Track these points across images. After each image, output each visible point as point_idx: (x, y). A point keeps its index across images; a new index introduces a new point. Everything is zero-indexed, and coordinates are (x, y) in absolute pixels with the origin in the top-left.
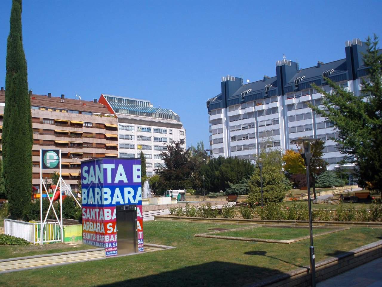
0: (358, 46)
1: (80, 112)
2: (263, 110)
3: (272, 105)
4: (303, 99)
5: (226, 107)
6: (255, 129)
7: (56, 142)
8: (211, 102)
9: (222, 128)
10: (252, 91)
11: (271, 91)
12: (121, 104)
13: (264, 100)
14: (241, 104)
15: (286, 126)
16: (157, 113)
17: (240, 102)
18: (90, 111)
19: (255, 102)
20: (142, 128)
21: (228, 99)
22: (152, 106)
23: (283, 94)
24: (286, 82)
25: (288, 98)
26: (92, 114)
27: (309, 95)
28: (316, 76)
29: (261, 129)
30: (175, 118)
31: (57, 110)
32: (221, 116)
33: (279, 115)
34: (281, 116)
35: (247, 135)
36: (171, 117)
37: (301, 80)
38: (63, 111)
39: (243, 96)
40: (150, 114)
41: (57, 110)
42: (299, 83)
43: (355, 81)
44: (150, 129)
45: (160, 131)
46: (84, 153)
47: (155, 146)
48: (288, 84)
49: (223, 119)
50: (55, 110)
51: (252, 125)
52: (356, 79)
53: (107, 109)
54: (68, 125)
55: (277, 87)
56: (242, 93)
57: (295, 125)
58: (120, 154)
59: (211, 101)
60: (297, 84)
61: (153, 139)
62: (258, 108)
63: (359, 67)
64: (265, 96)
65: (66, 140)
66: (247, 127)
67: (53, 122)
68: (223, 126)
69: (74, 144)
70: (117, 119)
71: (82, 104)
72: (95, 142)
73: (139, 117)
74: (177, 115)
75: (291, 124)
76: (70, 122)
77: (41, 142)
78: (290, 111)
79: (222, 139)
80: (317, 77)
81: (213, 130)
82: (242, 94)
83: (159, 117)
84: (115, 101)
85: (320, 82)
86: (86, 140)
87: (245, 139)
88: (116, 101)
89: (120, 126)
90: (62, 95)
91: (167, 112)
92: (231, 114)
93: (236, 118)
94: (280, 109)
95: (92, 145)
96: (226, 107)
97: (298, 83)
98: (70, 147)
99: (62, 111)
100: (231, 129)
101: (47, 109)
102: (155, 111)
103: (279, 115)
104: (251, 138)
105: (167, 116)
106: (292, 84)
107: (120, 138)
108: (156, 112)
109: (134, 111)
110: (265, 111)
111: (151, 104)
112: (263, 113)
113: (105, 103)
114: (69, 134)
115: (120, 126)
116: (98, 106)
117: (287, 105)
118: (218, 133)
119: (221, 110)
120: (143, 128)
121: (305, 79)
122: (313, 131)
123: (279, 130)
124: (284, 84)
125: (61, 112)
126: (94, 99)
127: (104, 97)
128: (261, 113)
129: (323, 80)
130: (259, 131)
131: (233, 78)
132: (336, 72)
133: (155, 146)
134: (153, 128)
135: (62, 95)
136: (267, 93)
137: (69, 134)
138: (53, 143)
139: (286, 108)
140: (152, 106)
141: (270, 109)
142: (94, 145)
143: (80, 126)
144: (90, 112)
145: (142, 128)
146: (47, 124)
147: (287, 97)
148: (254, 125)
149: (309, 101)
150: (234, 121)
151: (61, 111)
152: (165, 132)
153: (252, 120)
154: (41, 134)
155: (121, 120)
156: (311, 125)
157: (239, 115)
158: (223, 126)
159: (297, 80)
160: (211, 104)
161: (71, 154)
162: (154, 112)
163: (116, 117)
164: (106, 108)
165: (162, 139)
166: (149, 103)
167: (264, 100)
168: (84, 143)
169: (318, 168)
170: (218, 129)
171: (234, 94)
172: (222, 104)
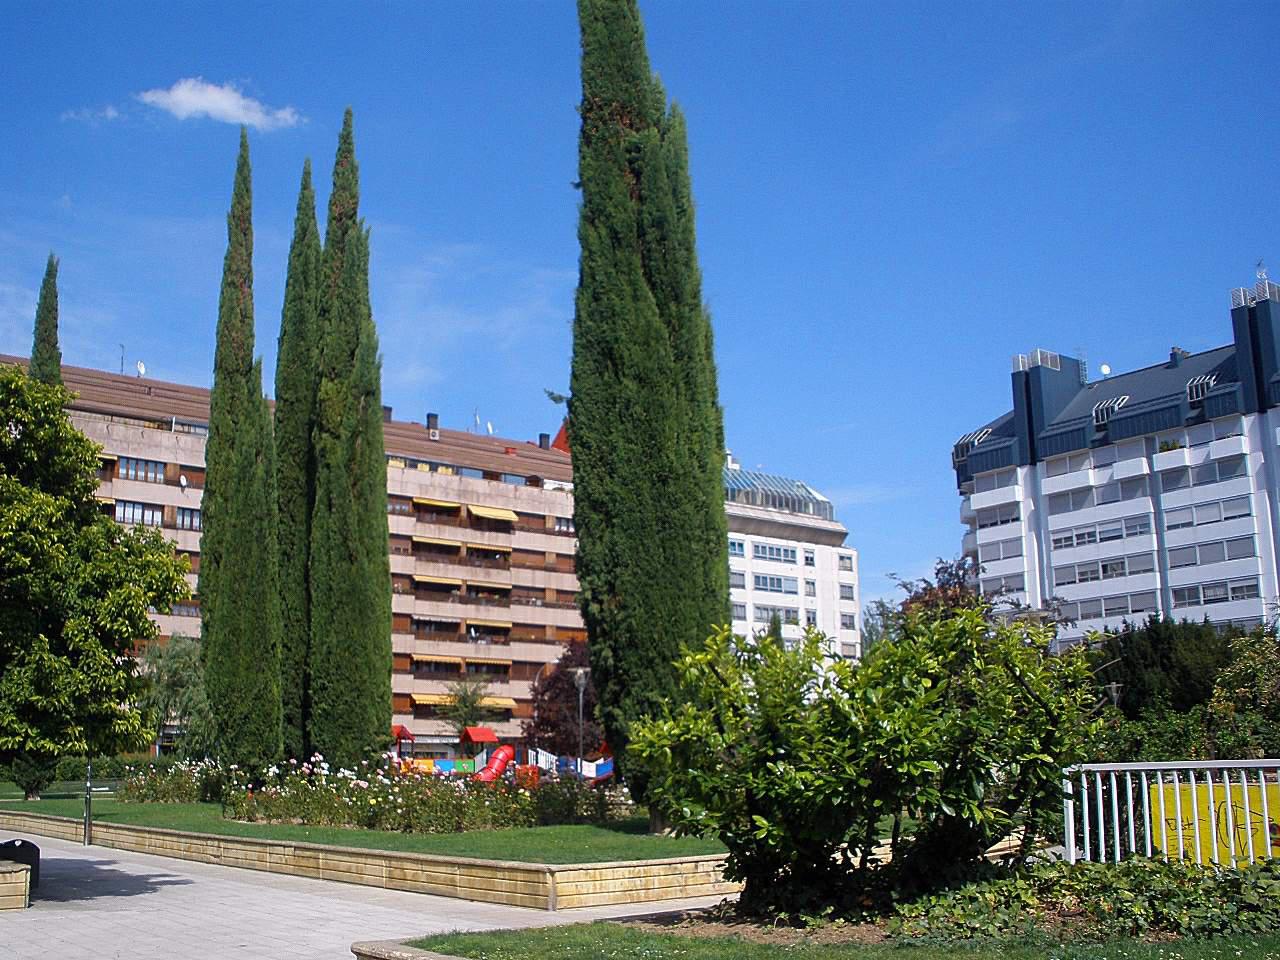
0: (1271, 305)
2: (1182, 471)
3: (1219, 449)
6: (1151, 539)
7: (417, 578)
8: (973, 445)
9: (1020, 539)
10: (1131, 403)
13: (1186, 432)
14: (1094, 448)
17: (1183, 422)
19: (1150, 441)
22: (736, 467)
23: (1033, 461)
29: (1173, 539)
30: (819, 510)
31: (419, 465)
32: (1183, 459)
34: (1259, 488)
36: (806, 506)
37: (1116, 408)
38: (440, 469)
41: (419, 465)
43: (1265, 415)
45: (774, 554)
46: (514, 624)
47: (758, 608)
49: (1021, 505)
50: (413, 464)
51: (1065, 538)
54: (461, 521)
55: (1016, 439)
62: (1164, 461)
63: (1043, 429)
66: (1121, 529)
67: (407, 508)
68: (1022, 528)
69: (478, 589)
74: (827, 500)
75: (1063, 557)
76: (469, 511)
78: (1131, 498)
79: (1021, 575)
81: (982, 546)
83: (767, 503)
85: (1178, 414)
87: (1086, 580)
92: (1054, 484)
93: (1079, 497)
94: (1024, 512)
96: (1033, 463)
97: (1103, 420)
98: (463, 601)
99: (436, 470)
100: (1225, 510)
106: (1179, 399)
108: (754, 485)
110: (1190, 470)
111: (734, 461)
112: (1089, 497)
114: (464, 552)
118: (1004, 558)
119: (1015, 471)
122: (1158, 574)
124: (1266, 371)
125: (435, 474)
126: (429, 416)
128: (1174, 478)
131: (1053, 358)
132: (991, 440)
133: (758, 608)
136: (1099, 428)
137: (464, 552)
138: (407, 585)
139: (1044, 505)
140: (736, 467)
142: (550, 597)
148: (1148, 525)
149: (1141, 478)
150: (995, 524)
151: (434, 467)
152: (790, 557)
153: (1142, 505)
156: (1019, 579)
157: (1089, 488)
158: (1022, 528)
160: (971, 452)
161: (469, 627)
165: (779, 580)
167: (1186, 432)
168: (515, 587)
170: (1003, 542)
171: (1059, 414)
172: (1016, 450)
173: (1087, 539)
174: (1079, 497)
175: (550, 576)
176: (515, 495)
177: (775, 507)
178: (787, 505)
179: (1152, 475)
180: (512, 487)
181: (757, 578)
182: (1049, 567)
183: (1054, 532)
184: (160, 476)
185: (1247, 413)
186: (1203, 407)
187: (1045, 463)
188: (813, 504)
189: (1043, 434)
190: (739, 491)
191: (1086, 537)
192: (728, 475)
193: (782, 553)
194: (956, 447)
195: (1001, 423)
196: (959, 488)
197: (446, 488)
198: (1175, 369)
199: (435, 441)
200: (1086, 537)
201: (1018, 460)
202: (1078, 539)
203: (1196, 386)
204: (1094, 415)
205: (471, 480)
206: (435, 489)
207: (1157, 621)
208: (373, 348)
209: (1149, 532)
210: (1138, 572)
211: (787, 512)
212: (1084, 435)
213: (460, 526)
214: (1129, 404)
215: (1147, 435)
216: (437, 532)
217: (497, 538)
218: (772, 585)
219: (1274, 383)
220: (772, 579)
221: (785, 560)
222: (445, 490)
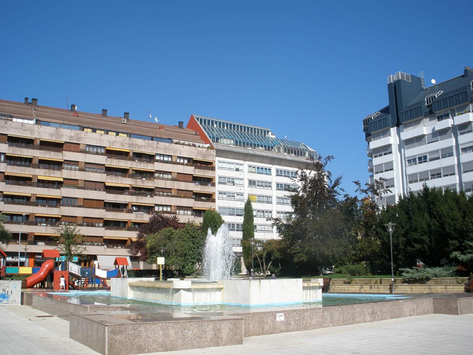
1: (152, 139)
2: (423, 136)
7: (107, 184)
12: (223, 131)
16: (281, 145)
18: (169, 137)
20: (256, 168)
26: (172, 142)
35: (439, 169)
39: (428, 103)
40: (269, 148)
44: (270, 170)
45: (260, 171)
49: (392, 145)
53: (199, 137)
56: (427, 99)
58: (219, 208)
59: (371, 118)
61: (274, 186)
65: (126, 182)
69: (140, 189)
70: (215, 151)
72: (176, 187)
73: (249, 150)
74: (314, 151)
76: (131, 240)
77: (81, 184)
81: (375, 166)
83: (285, 151)
84: (213, 125)
85: (466, 96)
86: (160, 184)
88: (215, 126)
89: (220, 162)
90: (125, 113)
91: (297, 146)
92: (409, 133)
95: (171, 193)
101: (94, 130)
107: (219, 183)
109: (244, 143)
111: (272, 134)
113: (198, 129)
114: (131, 172)
115: (220, 162)
116: (183, 131)
120: (258, 168)
123: (455, 185)
126: (179, 122)
130: (461, 161)
134: (274, 168)
135: (125, 113)
137: (131, 154)
141: (414, 139)
143: (151, 158)
145: (256, 168)
146: (67, 169)
151: (117, 134)
152: (268, 171)
153: (451, 142)
154: (80, 170)
155: (221, 153)
161: (133, 206)
162: (277, 145)
163: (212, 148)
164: (197, 135)
166: (268, 132)
168: (156, 187)
174: (419, 139)
175: (75, 176)
176: (157, 146)
180: (155, 142)
181: (278, 184)
183: (407, 158)
186: (431, 107)
187: (403, 125)
189: (402, 111)
191: (423, 159)
193: (290, 173)
197: (122, 143)
199: (125, 124)
200: (423, 159)
201: (390, 124)
205: (135, 139)
206: (117, 143)
207: (402, 199)
208: (373, 150)
209: (452, 155)
210: (447, 175)
211: (251, 149)
212: (421, 109)
213: (129, 160)
216: (117, 162)
217: (208, 173)
221: (284, 176)
222: (122, 144)
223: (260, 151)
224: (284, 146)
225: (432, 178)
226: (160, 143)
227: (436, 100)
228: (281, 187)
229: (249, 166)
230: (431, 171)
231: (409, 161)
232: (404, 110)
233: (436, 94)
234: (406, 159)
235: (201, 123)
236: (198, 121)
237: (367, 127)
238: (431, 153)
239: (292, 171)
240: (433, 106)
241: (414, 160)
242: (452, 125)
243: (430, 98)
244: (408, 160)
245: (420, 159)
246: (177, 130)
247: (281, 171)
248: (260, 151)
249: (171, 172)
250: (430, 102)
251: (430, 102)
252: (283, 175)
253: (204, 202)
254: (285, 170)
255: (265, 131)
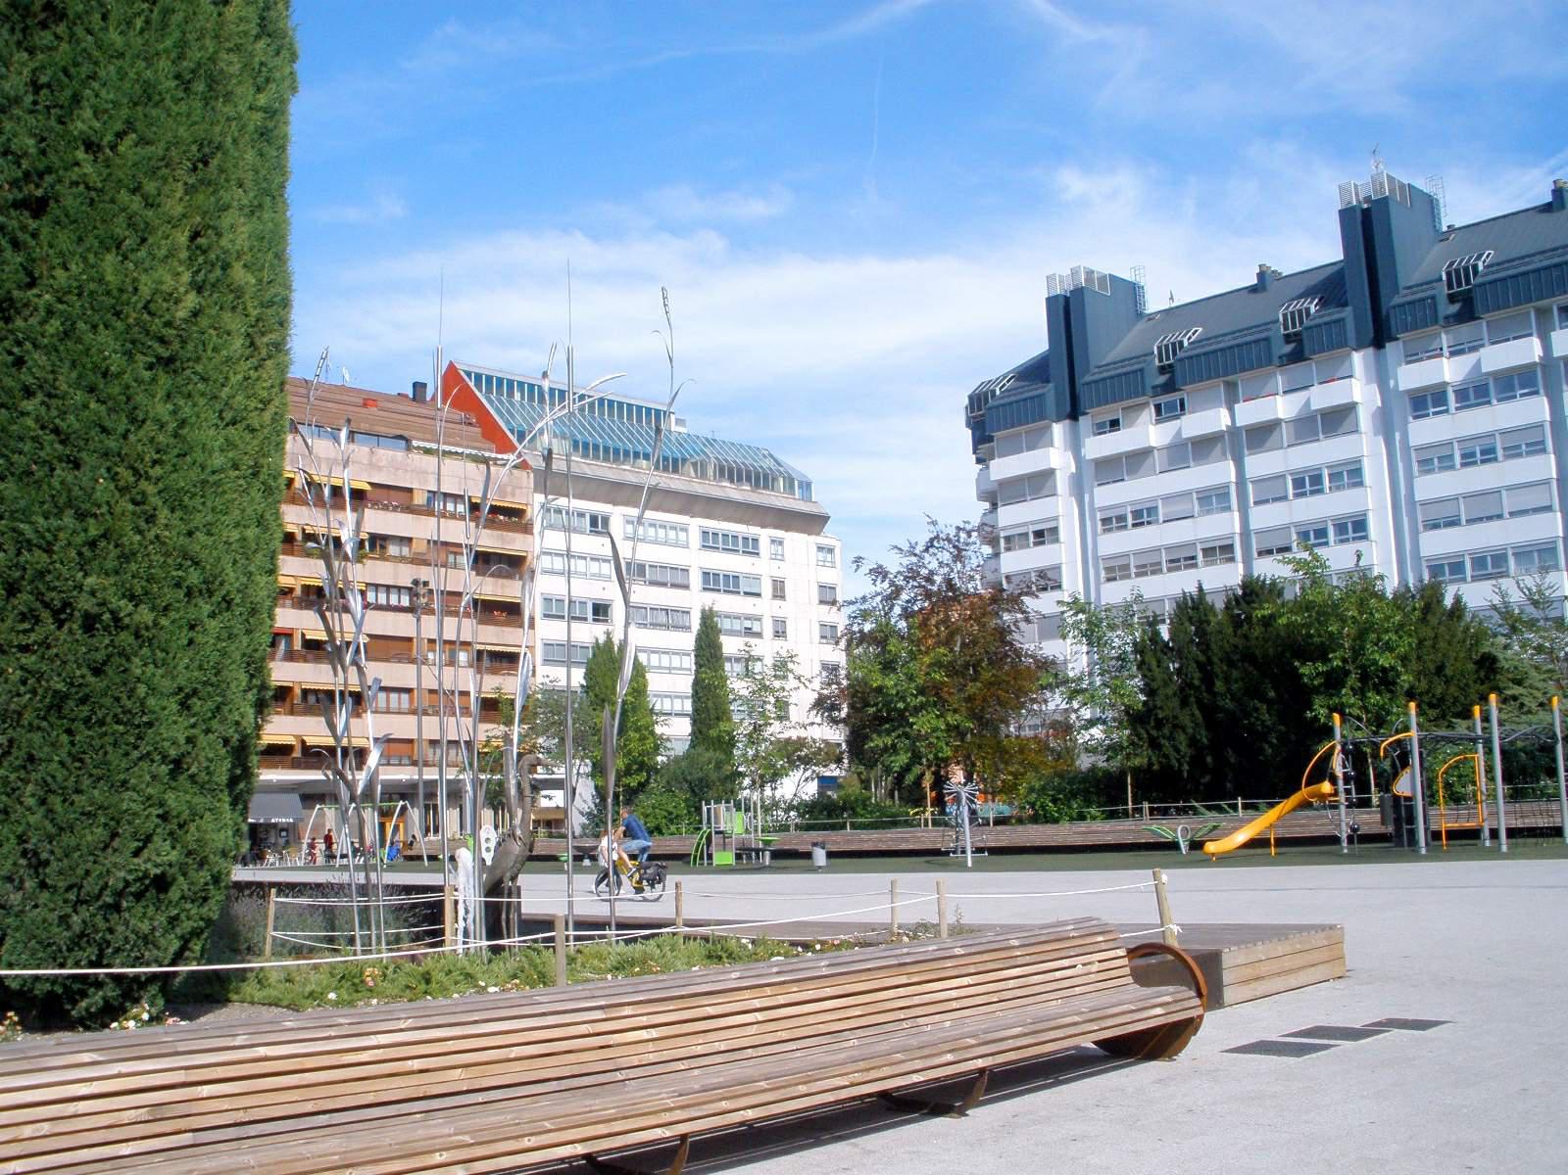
2: (1145, 453)
3: (1323, 396)
4: (1499, 356)
5: (1074, 415)
6: (1233, 519)
11: (997, 407)
15: (1403, 492)
16: (708, 457)
18: (399, 432)
19: (1231, 387)
21: (1084, 376)
23: (1379, 337)
24: (1396, 284)
25: (1412, 357)
27: (1531, 335)
28: (1246, 326)
32: (1275, 410)
33: (1365, 445)
39: (1161, 360)
40: (672, 465)
42: (1301, 322)
48: (1405, 292)
52: (1388, 345)
53: (478, 430)
56: (1159, 348)
57: (1156, 543)
60: (1291, 330)
61: (695, 579)
62: (1249, 413)
64: (1285, 355)
70: (532, 475)
71: (361, 401)
75: (1432, 486)
79: (1057, 568)
80: (1425, 287)
82: (1160, 353)
83: (722, 474)
84: (511, 394)
85: (1269, 348)
88: (517, 396)
93: (1135, 461)
102: (702, 451)
103: (1365, 445)
104: (1436, 526)
105: (749, 473)
110: (1283, 424)
117: (1093, 460)
121: (1200, 341)
124: (1384, 290)
126: (415, 385)
127: (462, 374)
128: (1261, 435)
129: (1282, 340)
130: (1253, 526)
134: (696, 524)
139: (1089, 473)
141: (1121, 458)
144: (401, 437)
147: (1406, 356)
152: (751, 547)
153: (1220, 471)
159: (1457, 271)
162: (698, 454)
164: (470, 424)
169: (1246, 722)
173: (1115, 524)
174: (1135, 461)
176: (370, 461)
177: (732, 481)
178: (749, 479)
179: (1234, 431)
181: (706, 574)
182: (1096, 558)
183: (1101, 509)
184: (405, 705)
185: (1058, 420)
186: (1173, 372)
187: (1400, 343)
188: (784, 478)
189: (1088, 378)
190: (684, 460)
191: (1143, 516)
192: (670, 440)
194: (971, 398)
195: (1026, 368)
196: (974, 453)
198: (1264, 294)
200: (1143, 516)
201: (1352, 342)
202: (1103, 525)
203: (1292, 313)
204: (1156, 352)
212: (1142, 377)
214: (1495, 261)
215: (1539, 303)
218: (727, 584)
219: (1394, 307)
220: (726, 576)
221: (724, 549)
223: (643, 474)
224: (717, 458)
225: (1170, 570)
226: (381, 452)
227: (1187, 354)
228: (717, 582)
229: (819, 548)
230: (1168, 549)
231: (1105, 521)
232: (1094, 374)
233: (1185, 335)
234: (1099, 516)
235: (478, 384)
236: (470, 379)
237: (982, 416)
238: (1167, 499)
239: (746, 535)
240: (1178, 367)
241: (1121, 518)
242: (1227, 426)
243: (1167, 346)
244: (1203, 550)
245: (1137, 514)
246: (409, 409)
247: (745, 539)
248: (643, 474)
249: (410, 539)
250: (1168, 358)
251: (1168, 358)
252: (721, 546)
253: (504, 629)
254: (725, 532)
255: (658, 412)
